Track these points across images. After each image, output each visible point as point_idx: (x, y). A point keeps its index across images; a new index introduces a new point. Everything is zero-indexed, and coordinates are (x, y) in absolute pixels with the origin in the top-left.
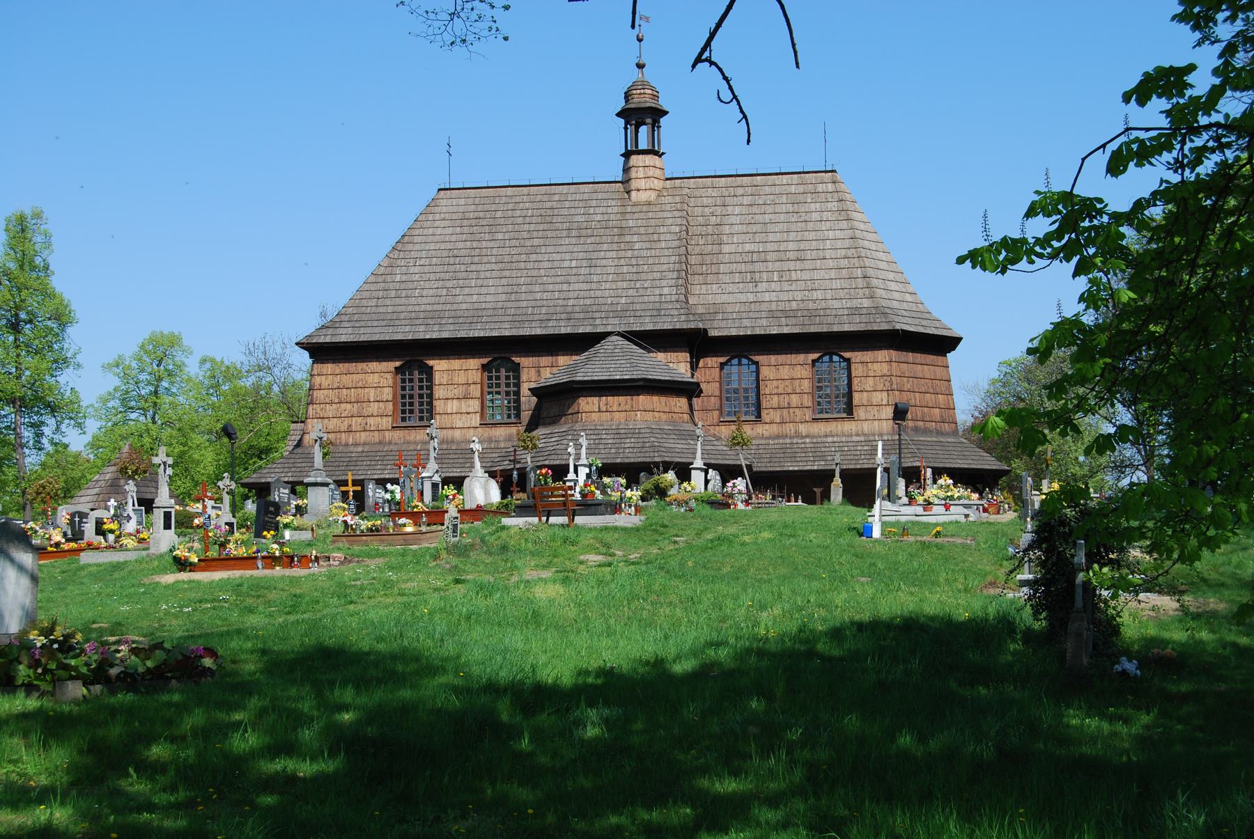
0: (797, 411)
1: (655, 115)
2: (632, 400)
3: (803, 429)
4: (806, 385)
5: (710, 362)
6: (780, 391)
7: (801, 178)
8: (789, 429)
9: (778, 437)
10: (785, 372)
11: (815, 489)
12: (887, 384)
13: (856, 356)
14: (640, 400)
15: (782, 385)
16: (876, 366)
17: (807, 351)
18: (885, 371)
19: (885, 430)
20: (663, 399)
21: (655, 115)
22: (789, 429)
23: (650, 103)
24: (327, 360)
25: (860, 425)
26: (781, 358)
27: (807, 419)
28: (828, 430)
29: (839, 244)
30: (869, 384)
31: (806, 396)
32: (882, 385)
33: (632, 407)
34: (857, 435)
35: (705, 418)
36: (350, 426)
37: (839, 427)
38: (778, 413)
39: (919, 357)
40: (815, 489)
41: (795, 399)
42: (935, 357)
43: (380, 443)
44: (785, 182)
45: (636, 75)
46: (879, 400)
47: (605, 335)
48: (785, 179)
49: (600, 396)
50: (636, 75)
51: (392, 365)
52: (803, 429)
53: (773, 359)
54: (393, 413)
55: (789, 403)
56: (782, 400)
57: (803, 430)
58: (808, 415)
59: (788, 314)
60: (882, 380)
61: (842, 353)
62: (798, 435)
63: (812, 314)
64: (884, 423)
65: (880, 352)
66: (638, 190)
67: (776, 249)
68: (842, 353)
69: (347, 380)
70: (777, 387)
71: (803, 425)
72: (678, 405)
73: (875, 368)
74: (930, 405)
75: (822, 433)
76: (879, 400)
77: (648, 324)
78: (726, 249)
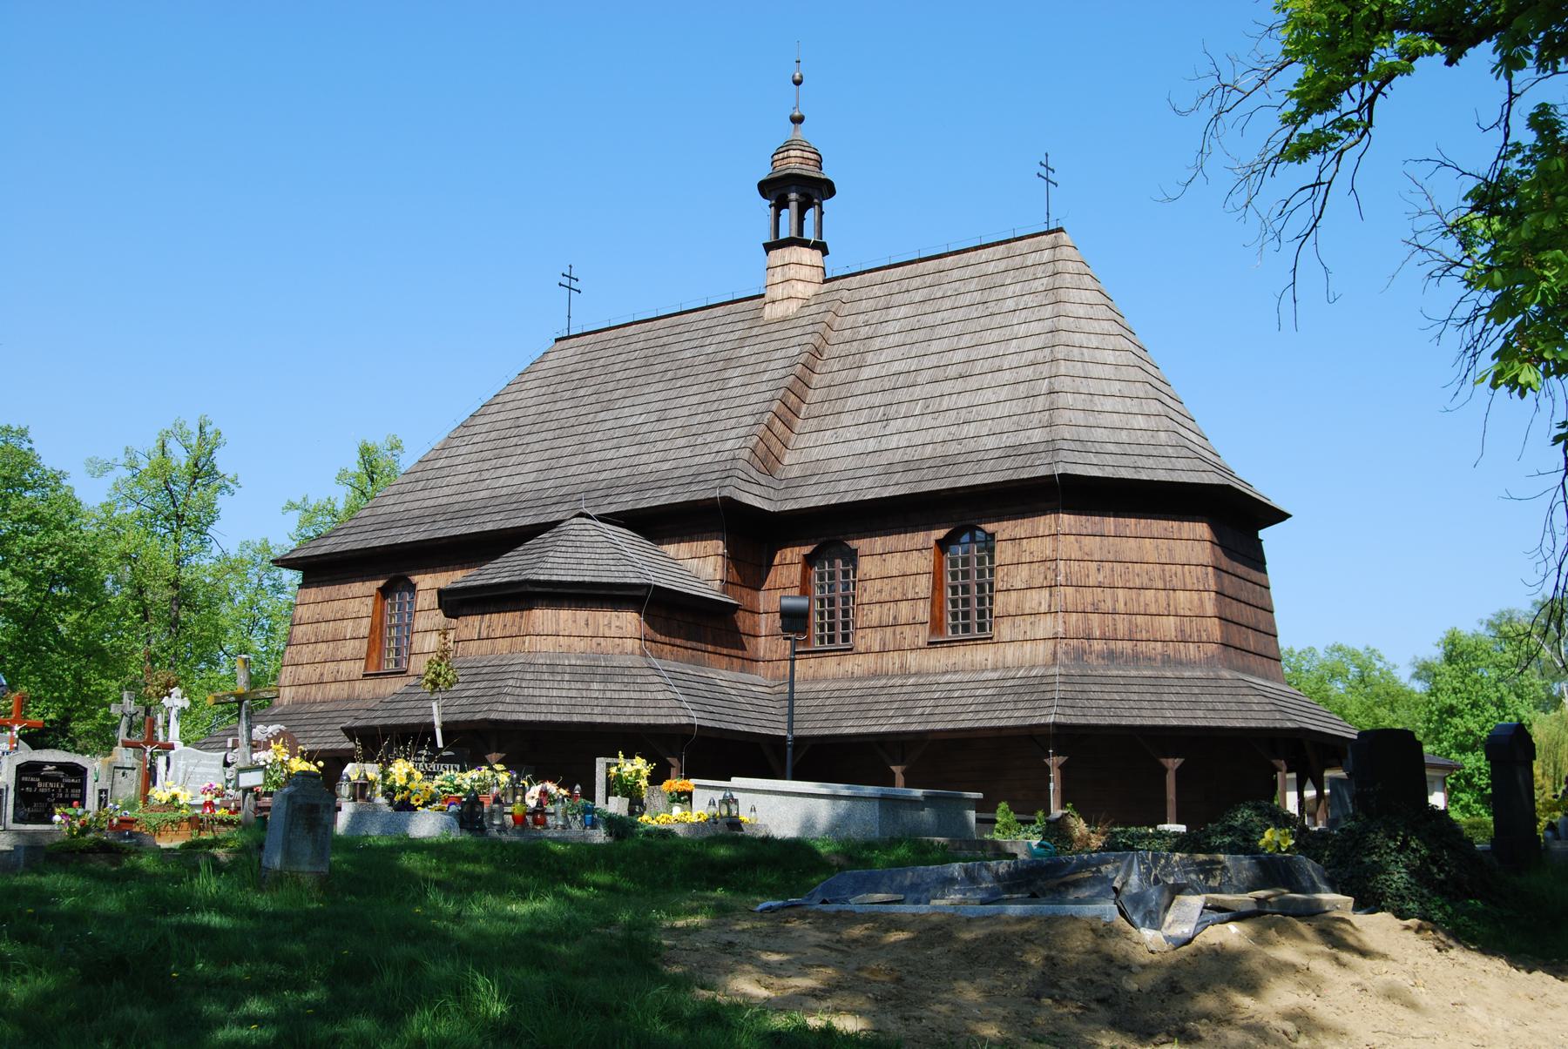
0: (907, 630)
1: (776, 189)
2: (521, 617)
3: (913, 660)
4: (924, 585)
5: (789, 555)
6: (885, 597)
7: (1009, 249)
8: (892, 661)
9: (875, 675)
10: (894, 564)
11: (893, 768)
12: (1050, 575)
13: (1003, 529)
14: (562, 616)
15: (887, 586)
16: (1034, 545)
17: (929, 526)
18: (1049, 553)
19: (1040, 660)
20: (582, 615)
21: (776, 189)
22: (892, 661)
23: (810, 171)
24: (313, 583)
25: (1001, 651)
26: (892, 541)
27: (920, 644)
28: (951, 661)
29: (1030, 343)
30: (1021, 576)
31: (921, 603)
32: (1042, 576)
33: (520, 630)
34: (995, 669)
35: (774, 648)
36: (322, 675)
37: (969, 657)
38: (879, 634)
39: (1132, 524)
40: (893, 768)
41: (905, 610)
42: (1176, 524)
43: (348, 699)
44: (984, 258)
45: (789, 132)
46: (1035, 604)
47: (604, 518)
48: (984, 254)
49: (483, 614)
50: (789, 132)
51: (373, 586)
52: (913, 660)
53: (879, 543)
54: (368, 655)
55: (895, 618)
56: (886, 611)
57: (913, 664)
58: (924, 635)
59: (909, 466)
60: (1042, 569)
61: (983, 526)
62: (905, 673)
63: (948, 461)
64: (1041, 645)
65: (1043, 518)
66: (773, 302)
67: (935, 364)
68: (983, 526)
69: (328, 610)
70: (880, 591)
71: (914, 654)
72: (615, 623)
73: (1034, 548)
74: (1153, 610)
75: (941, 666)
76: (1035, 604)
77: (626, 502)
78: (866, 373)
